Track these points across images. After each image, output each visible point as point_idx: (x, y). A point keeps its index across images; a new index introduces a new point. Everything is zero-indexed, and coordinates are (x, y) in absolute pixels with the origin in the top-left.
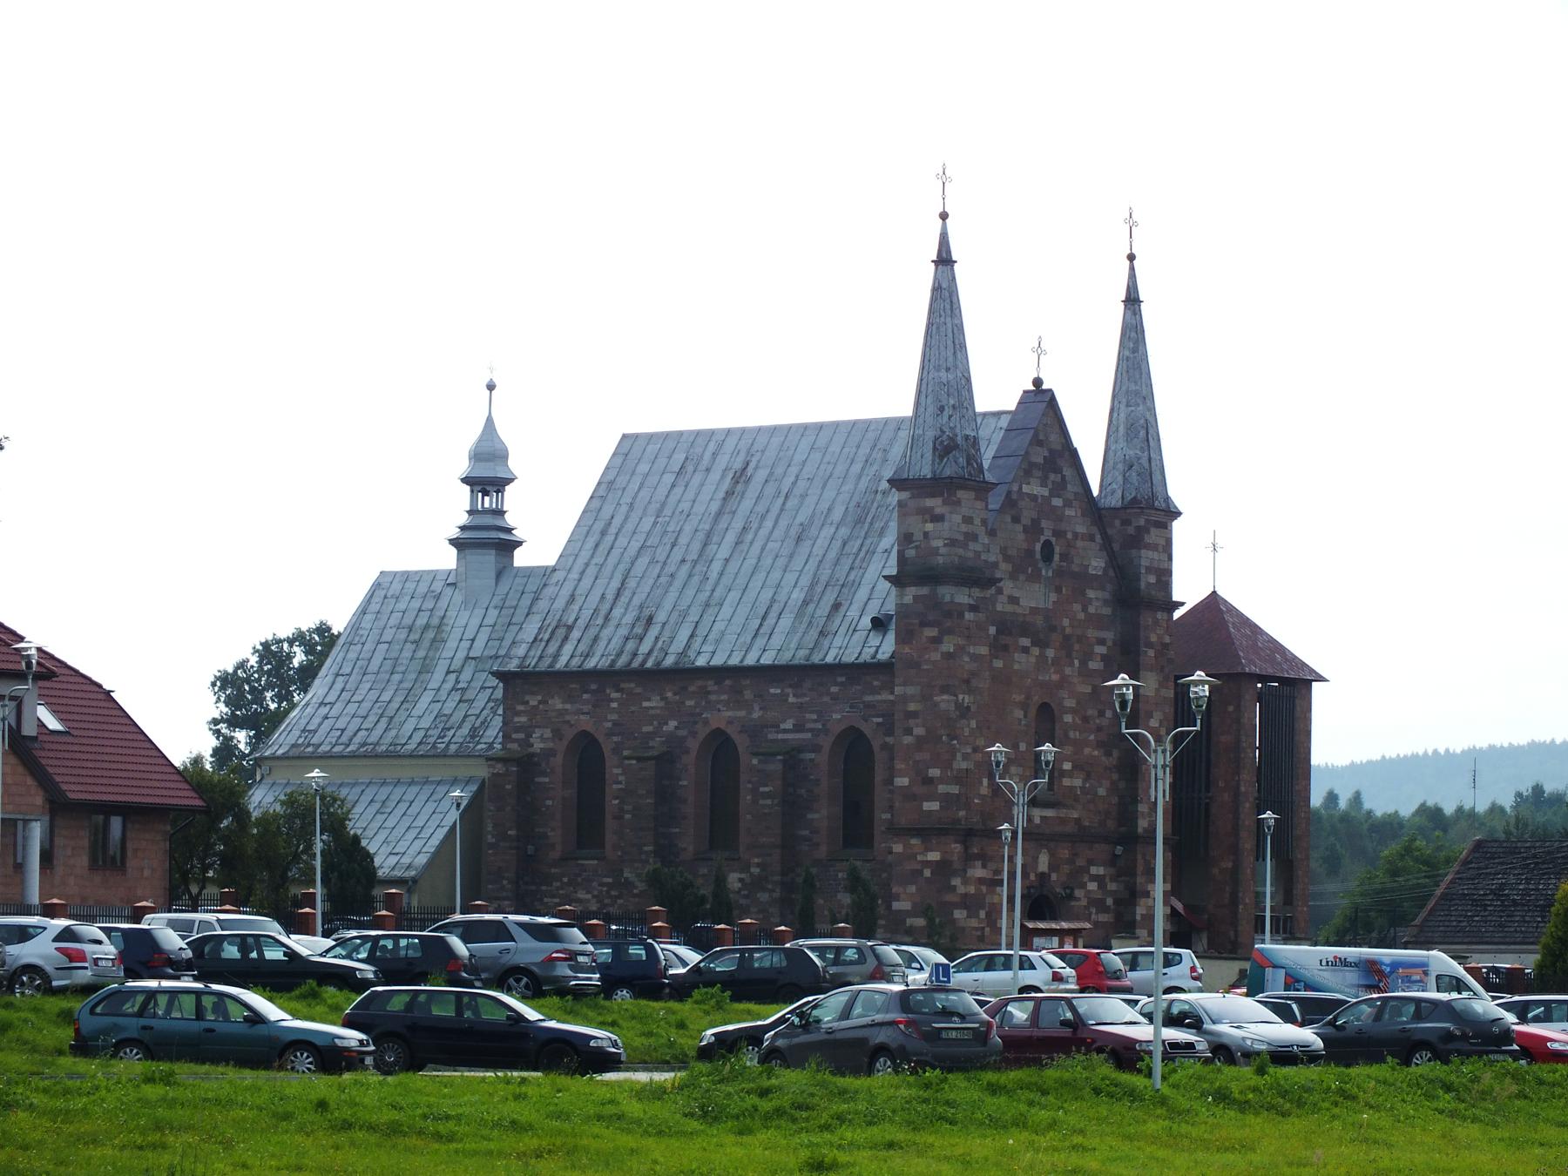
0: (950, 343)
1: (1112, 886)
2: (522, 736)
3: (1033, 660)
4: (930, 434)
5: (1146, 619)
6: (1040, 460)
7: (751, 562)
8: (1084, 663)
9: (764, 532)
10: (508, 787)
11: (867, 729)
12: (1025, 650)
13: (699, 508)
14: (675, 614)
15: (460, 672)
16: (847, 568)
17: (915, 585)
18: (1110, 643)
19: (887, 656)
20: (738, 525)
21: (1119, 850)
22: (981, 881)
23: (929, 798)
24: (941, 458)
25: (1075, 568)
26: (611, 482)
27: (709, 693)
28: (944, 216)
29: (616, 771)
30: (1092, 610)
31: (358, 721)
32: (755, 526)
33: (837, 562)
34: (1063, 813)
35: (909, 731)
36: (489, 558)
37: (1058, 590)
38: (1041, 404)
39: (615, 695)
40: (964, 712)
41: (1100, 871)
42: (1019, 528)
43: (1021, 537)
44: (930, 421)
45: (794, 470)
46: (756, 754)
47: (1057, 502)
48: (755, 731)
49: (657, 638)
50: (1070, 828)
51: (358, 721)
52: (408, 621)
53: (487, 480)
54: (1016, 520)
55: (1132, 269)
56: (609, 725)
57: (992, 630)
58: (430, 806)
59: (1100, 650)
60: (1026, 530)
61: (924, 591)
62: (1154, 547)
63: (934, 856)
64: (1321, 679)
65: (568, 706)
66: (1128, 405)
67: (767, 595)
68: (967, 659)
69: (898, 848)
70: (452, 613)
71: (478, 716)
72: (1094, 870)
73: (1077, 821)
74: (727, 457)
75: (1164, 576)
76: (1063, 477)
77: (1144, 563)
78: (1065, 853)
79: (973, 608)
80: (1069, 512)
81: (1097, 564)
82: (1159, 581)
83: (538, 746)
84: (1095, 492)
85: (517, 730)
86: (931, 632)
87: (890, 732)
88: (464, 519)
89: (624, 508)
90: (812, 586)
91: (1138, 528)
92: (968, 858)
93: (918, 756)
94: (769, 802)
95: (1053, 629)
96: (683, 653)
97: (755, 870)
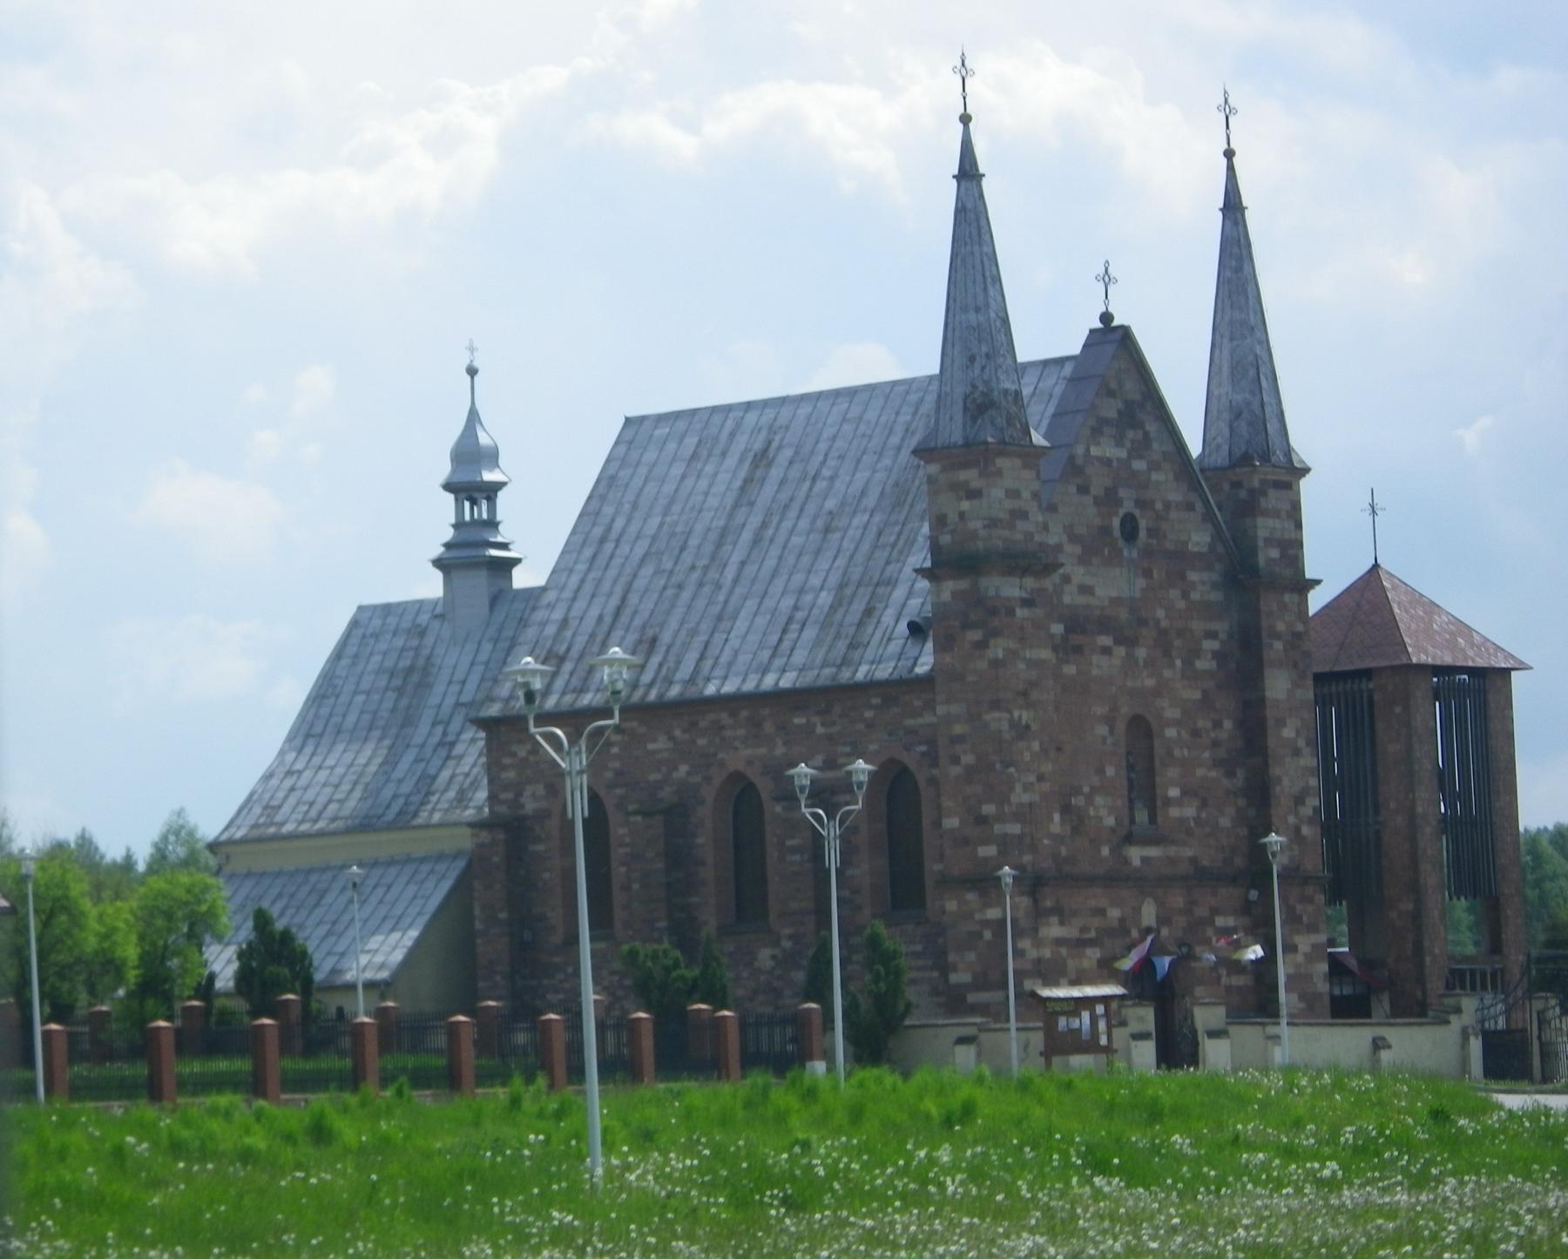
0: (979, 277)
3: (1117, 662)
4: (960, 391)
5: (1268, 603)
6: (1113, 414)
7: (770, 563)
8: (1188, 663)
9: (787, 524)
11: (910, 760)
12: (1106, 651)
13: (713, 502)
14: (683, 633)
15: (448, 723)
16: (882, 562)
18: (1223, 636)
19: (926, 668)
20: (755, 521)
22: (1059, 942)
23: (985, 842)
24: (974, 419)
25: (1169, 546)
26: (613, 478)
27: (722, 728)
29: (622, 831)
30: (1195, 596)
31: (328, 790)
32: (775, 519)
33: (870, 558)
34: (1172, 851)
35: (955, 760)
36: (480, 582)
37: (1147, 574)
38: (1113, 343)
40: (1023, 731)
41: (1230, 922)
42: (1088, 500)
43: (1092, 511)
45: (822, 446)
47: (1139, 465)
49: (661, 665)
51: (328, 790)
52: (389, 663)
53: (472, 486)
54: (1083, 490)
55: (1231, 169)
57: (1057, 629)
58: (412, 888)
59: (1210, 645)
60: (1097, 502)
61: (963, 584)
62: (1276, 514)
66: (1232, 339)
67: (789, 602)
68: (1022, 666)
69: (951, 906)
70: (440, 650)
71: (467, 775)
72: (1220, 921)
73: (1193, 860)
74: (746, 437)
75: (1292, 549)
76: (1146, 434)
77: (1262, 533)
78: (1177, 900)
79: (1027, 603)
80: (1155, 476)
81: (1199, 539)
82: (1283, 555)
83: (530, 806)
84: (1195, 447)
86: (975, 635)
87: (935, 763)
88: (448, 534)
89: (627, 507)
90: (842, 586)
94: (797, 858)
95: (1142, 622)
96: (692, 680)
97: (786, 944)
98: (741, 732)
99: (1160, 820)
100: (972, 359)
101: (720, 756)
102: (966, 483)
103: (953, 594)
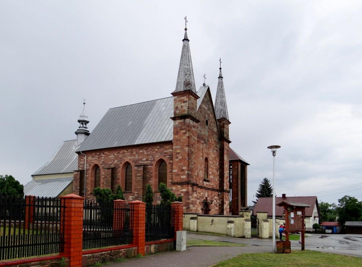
1: (218, 201)
2: (82, 166)
4: (183, 81)
10: (78, 177)
17: (179, 119)
21: (220, 193)
22: (196, 197)
28: (186, 30)
35: (177, 158)
39: (103, 155)
44: (183, 77)
46: (136, 166)
48: (135, 161)
50: (211, 187)
56: (102, 162)
61: (182, 121)
63: (184, 190)
64: (249, 165)
65: (92, 159)
73: (212, 186)
85: (81, 165)
86: (184, 131)
91: (224, 124)
92: (193, 191)
93: (180, 164)
94: (139, 178)
97: (136, 195)
98: (129, 154)
99: (208, 177)
100: (186, 74)
101: (124, 159)
102: (183, 100)
103: (179, 123)
